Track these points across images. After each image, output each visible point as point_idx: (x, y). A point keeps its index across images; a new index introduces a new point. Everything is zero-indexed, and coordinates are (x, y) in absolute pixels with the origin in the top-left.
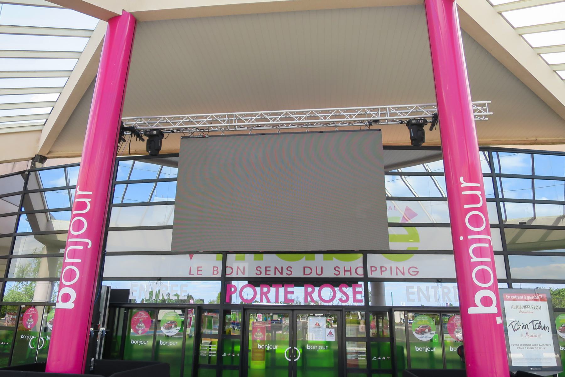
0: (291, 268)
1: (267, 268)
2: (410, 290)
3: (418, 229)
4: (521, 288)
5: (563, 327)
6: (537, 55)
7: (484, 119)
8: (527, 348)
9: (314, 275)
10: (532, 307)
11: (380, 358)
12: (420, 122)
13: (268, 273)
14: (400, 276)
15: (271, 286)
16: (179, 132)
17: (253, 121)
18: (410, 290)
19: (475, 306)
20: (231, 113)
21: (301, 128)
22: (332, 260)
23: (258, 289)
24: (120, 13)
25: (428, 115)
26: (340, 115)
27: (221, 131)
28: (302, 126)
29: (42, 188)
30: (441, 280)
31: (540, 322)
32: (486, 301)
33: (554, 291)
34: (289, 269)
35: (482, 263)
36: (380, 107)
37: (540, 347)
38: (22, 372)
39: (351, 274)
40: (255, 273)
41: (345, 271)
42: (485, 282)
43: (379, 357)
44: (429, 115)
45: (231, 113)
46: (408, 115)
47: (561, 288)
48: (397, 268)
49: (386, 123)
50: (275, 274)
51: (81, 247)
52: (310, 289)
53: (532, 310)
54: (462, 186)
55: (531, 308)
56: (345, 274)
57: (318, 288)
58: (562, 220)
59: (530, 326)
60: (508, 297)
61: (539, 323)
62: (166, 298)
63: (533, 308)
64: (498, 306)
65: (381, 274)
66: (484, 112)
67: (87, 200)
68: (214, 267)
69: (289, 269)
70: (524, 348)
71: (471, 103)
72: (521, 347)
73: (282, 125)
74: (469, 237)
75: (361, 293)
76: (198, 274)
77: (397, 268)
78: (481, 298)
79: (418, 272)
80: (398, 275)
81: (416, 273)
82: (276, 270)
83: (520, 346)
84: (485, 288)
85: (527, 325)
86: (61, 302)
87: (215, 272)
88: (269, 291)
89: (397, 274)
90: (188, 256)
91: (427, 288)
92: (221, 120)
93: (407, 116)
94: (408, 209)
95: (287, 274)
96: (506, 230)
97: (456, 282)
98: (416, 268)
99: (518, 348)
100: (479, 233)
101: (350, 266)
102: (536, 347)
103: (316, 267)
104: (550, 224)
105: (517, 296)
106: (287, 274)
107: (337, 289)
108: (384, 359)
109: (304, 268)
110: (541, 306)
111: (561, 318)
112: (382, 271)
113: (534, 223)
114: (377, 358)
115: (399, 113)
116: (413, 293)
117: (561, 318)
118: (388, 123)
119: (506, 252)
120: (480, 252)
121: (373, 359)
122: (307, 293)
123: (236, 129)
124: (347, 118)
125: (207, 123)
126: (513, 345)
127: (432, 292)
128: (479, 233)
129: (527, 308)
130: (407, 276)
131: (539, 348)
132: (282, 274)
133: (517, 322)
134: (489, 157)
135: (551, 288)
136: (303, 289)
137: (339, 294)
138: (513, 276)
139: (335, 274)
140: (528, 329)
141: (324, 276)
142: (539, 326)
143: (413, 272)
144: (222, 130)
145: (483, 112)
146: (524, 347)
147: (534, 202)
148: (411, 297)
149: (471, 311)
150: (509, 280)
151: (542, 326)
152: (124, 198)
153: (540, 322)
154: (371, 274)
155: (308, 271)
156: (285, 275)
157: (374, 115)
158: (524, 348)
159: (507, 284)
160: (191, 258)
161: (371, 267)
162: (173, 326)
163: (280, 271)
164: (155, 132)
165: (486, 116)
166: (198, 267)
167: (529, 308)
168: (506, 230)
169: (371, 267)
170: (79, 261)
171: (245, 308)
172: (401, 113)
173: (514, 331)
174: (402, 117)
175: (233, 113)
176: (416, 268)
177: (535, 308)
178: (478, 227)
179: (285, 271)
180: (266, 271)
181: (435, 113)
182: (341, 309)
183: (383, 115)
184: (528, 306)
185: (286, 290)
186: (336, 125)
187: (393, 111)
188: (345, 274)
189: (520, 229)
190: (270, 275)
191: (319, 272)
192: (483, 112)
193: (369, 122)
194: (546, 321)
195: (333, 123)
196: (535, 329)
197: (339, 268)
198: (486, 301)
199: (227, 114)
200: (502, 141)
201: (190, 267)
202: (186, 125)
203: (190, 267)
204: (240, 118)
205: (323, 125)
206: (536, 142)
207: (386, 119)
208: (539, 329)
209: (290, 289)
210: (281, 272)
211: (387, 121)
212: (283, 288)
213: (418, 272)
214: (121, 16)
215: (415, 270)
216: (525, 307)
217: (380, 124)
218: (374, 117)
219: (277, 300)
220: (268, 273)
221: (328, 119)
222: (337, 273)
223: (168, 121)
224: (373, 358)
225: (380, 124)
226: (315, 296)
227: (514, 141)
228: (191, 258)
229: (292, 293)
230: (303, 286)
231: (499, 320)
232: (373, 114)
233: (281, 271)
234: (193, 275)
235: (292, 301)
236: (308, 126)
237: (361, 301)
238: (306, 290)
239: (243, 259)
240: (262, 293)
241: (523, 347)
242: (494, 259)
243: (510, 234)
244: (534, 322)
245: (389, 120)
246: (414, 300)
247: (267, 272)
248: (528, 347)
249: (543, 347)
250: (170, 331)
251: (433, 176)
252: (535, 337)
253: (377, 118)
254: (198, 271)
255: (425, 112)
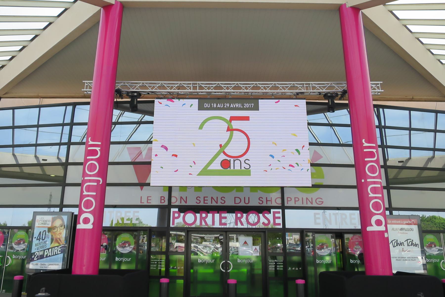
1: (205, 198)
3: (323, 168)
4: (399, 215)
5: (429, 244)
6: (415, 38)
7: (377, 94)
8: (402, 260)
9: (242, 204)
10: (407, 230)
11: (294, 269)
12: (334, 95)
13: (206, 202)
14: (309, 205)
15: (209, 213)
16: (153, 93)
18: (317, 216)
19: (371, 225)
20: (196, 82)
21: (247, 95)
22: (257, 192)
23: (198, 215)
24: (113, 2)
25: (339, 90)
27: (187, 94)
28: (247, 93)
30: (340, 208)
31: (413, 240)
32: (379, 223)
33: (426, 218)
34: (223, 199)
35: (376, 198)
36: (305, 82)
37: (412, 259)
38: (57, 274)
40: (220, 203)
41: (267, 201)
42: (378, 210)
43: (293, 268)
44: (340, 90)
45: (196, 82)
46: (326, 90)
47: (432, 215)
48: (307, 199)
49: (309, 94)
50: (212, 203)
51: (96, 184)
52: (239, 215)
53: (407, 232)
54: (364, 145)
55: (406, 230)
56: (267, 203)
57: (183, 214)
58: (430, 163)
59: (405, 243)
60: (389, 222)
61: (411, 241)
62: (120, 222)
63: (408, 230)
64: (386, 226)
66: (378, 89)
67: (98, 149)
69: (223, 199)
70: (400, 260)
71: (370, 83)
72: (399, 259)
73: (234, 92)
74: (368, 180)
75: (279, 218)
76: (147, 202)
77: (307, 199)
78: (376, 220)
79: (323, 202)
80: (304, 204)
81: (321, 203)
82: (216, 201)
83: (397, 259)
84: (378, 214)
85: (403, 242)
86: (82, 223)
87: (163, 201)
88: (207, 216)
89: (307, 203)
90: (139, 187)
91: (330, 214)
92: (186, 86)
94: (315, 152)
95: (221, 202)
96: (389, 170)
97: (358, 210)
98: (322, 199)
99: (396, 260)
100: (374, 178)
101: (267, 197)
102: (410, 259)
103: (245, 198)
104: (421, 165)
105: (396, 221)
106: (221, 202)
107: (261, 215)
108: (297, 269)
109: (235, 198)
110: (413, 229)
111: (427, 238)
112: (295, 201)
113: (409, 165)
114: (291, 269)
116: (319, 218)
117: (427, 238)
118: (311, 94)
119: (388, 188)
120: (374, 190)
121: (288, 270)
122: (237, 218)
123: (198, 94)
126: (393, 257)
127: (333, 217)
128: (374, 178)
129: (403, 230)
130: (315, 205)
131: (412, 260)
132: (217, 203)
133: (396, 240)
134: (377, 111)
135: (423, 216)
137: (262, 219)
138: (394, 205)
139: (259, 203)
140: (404, 246)
141: (251, 204)
142: (412, 243)
143: (319, 202)
144: (187, 94)
145: (377, 90)
146: (401, 259)
147: (410, 148)
148: (318, 221)
149: (369, 229)
150: (391, 209)
151: (413, 244)
152: (63, 133)
153: (413, 240)
154: (288, 203)
155: (238, 200)
156: (219, 204)
158: (400, 260)
159: (389, 211)
160: (142, 189)
161: (287, 198)
162: (127, 245)
163: (216, 200)
165: (378, 92)
166: (148, 197)
167: (405, 230)
168: (389, 170)
170: (95, 194)
171: (188, 230)
173: (394, 247)
174: (321, 91)
175: (197, 82)
176: (322, 199)
177: (409, 230)
178: (373, 174)
179: (219, 200)
180: (204, 200)
181: (344, 89)
182: (264, 230)
183: (307, 89)
184: (404, 228)
186: (273, 94)
189: (398, 169)
191: (247, 202)
192: (377, 90)
193: (296, 93)
194: (417, 240)
196: (409, 246)
198: (379, 223)
199: (192, 82)
200: (387, 98)
201: (141, 197)
203: (141, 197)
206: (413, 100)
208: (412, 245)
209: (223, 215)
211: (309, 93)
212: (218, 214)
213: (323, 202)
214: (114, 4)
216: (401, 229)
219: (213, 223)
220: (206, 202)
224: (289, 268)
225: (304, 94)
226: (244, 220)
227: (396, 98)
228: (142, 189)
229: (225, 218)
230: (233, 213)
231: (386, 235)
233: (182, 199)
234: (144, 203)
235: (225, 224)
237: (279, 224)
238: (236, 216)
240: (201, 218)
241: (400, 259)
242: (63, 13)
243: (392, 173)
244: (408, 241)
245: (311, 92)
246: (319, 224)
248: (404, 259)
249: (414, 259)
250: (124, 250)
251: (334, 126)
252: (409, 251)
253: (303, 91)
254: (148, 200)
255: (336, 87)
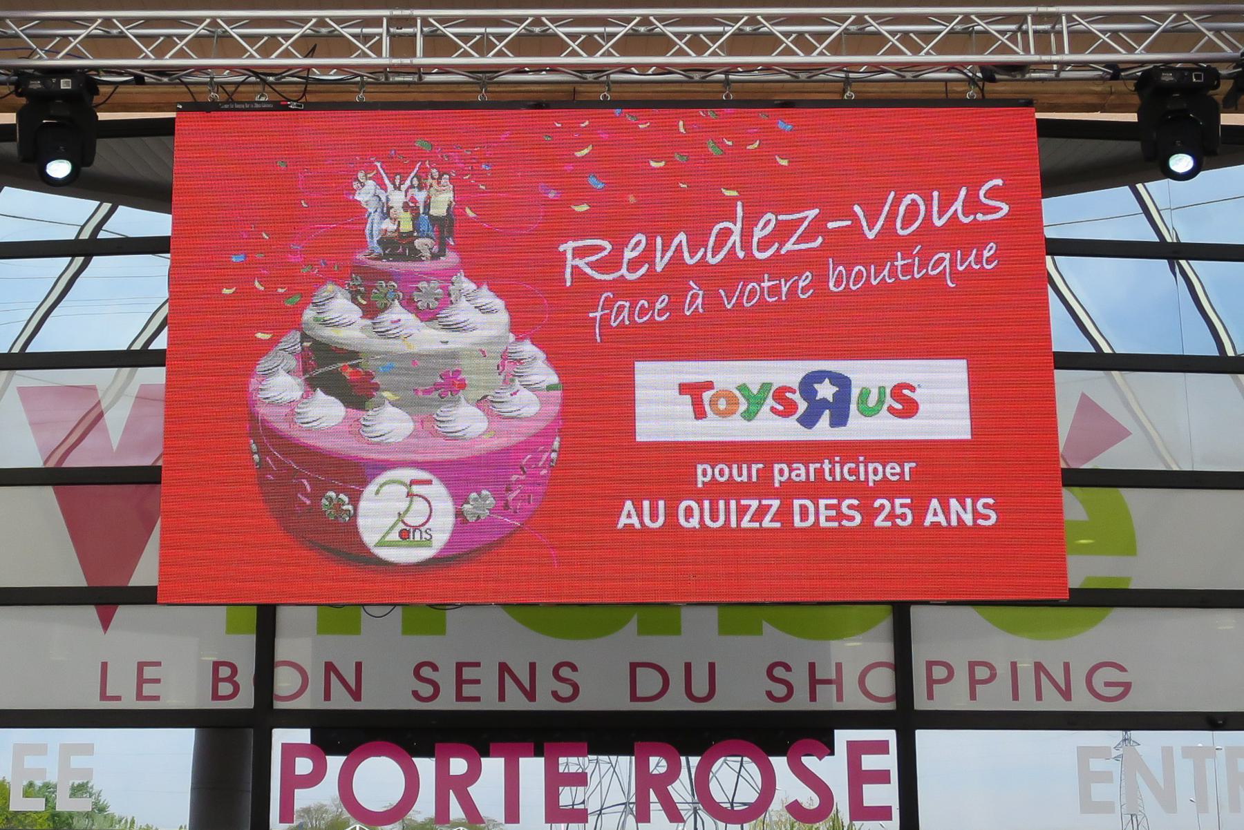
0: (574, 668)
1: (465, 669)
2: (870, 762)
9: (676, 701)
13: (468, 690)
14: (1053, 702)
15: (487, 754)
16: (166, 80)
17: (287, 49)
20: (407, 12)
23: (426, 766)
26: (650, 35)
29: (1230, 353)
39: (840, 697)
41: (814, 682)
45: (407, 12)
46: (1148, 50)
49: (1052, 75)
50: (502, 697)
52: (657, 765)
56: (813, 698)
65: (973, 696)
68: (217, 665)
75: (881, 777)
76: (140, 696)
77: (1039, 667)
79: (1127, 686)
82: (1044, 678)
88: (474, 773)
89: (1039, 697)
90: (90, 612)
91: (1167, 752)
92: (354, 36)
93: (1139, 55)
103: (688, 667)
107: (779, 763)
109: (634, 666)
112: (973, 682)
115: (1209, 30)
124: (570, 55)
125: (89, 56)
127: (1184, 770)
130: (1082, 702)
132: (531, 695)
136: (625, 763)
137: (789, 787)
143: (1108, 684)
144: (358, 79)
154: (930, 696)
155: (649, 682)
156: (544, 703)
157: (1004, 39)
160: (106, 622)
161: (930, 665)
163: (352, 681)
164: (65, 84)
166: (141, 666)
169: (632, 664)
172: (1115, 34)
174: (1123, 56)
175: (417, 12)
176: (1122, 669)
179: (546, 684)
180: (460, 682)
185: (551, 769)
186: (847, 78)
187: (1081, 24)
188: (813, 698)
190: (477, 699)
191: (701, 688)
195: (840, 67)
197: (435, 668)
199: (386, 13)
201: (104, 666)
202: (96, 57)
203: (104, 666)
204: (226, 31)
205: (792, 73)
207: (1052, 63)
209: (569, 764)
210: (353, 686)
212: (540, 761)
213: (1127, 686)
215: (1114, 675)
217: (1027, 76)
218: (1004, 49)
220: (468, 690)
221: (821, 54)
222: (780, 690)
223: (9, 32)
225: (1027, 76)
228: (106, 622)
232: (1100, 31)
233: (352, 683)
234: (118, 698)
236: (851, 75)
238: (642, 767)
239: (354, 628)
240: (445, 782)
247: (145, 686)
254: (141, 681)
